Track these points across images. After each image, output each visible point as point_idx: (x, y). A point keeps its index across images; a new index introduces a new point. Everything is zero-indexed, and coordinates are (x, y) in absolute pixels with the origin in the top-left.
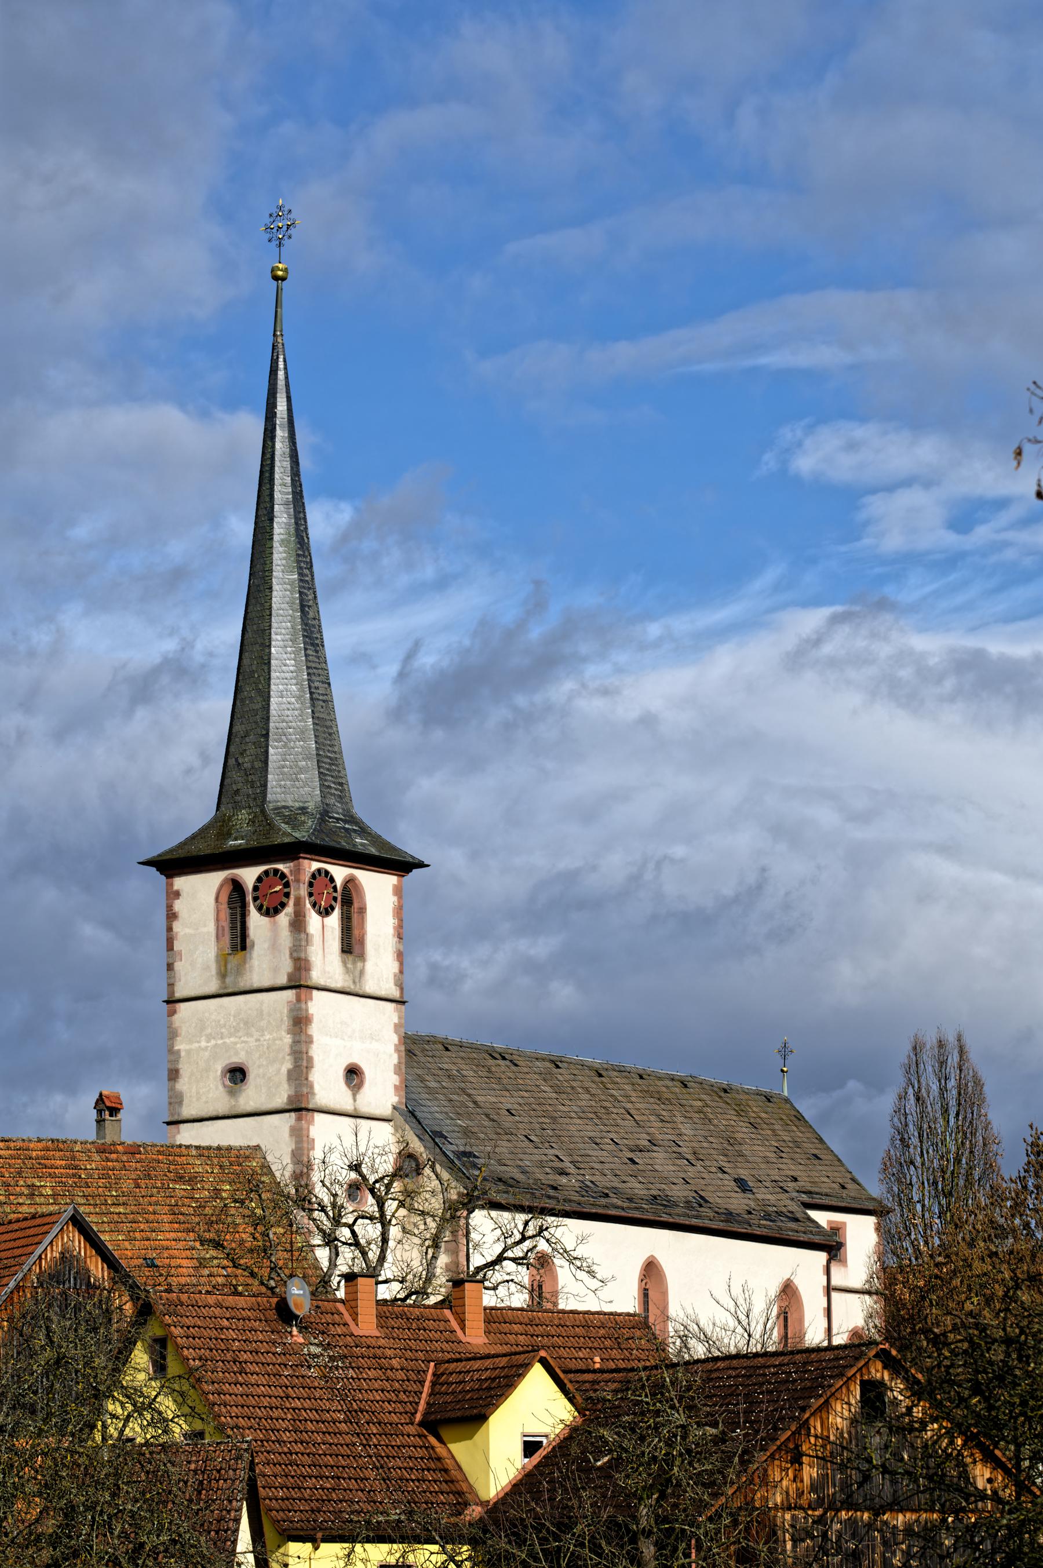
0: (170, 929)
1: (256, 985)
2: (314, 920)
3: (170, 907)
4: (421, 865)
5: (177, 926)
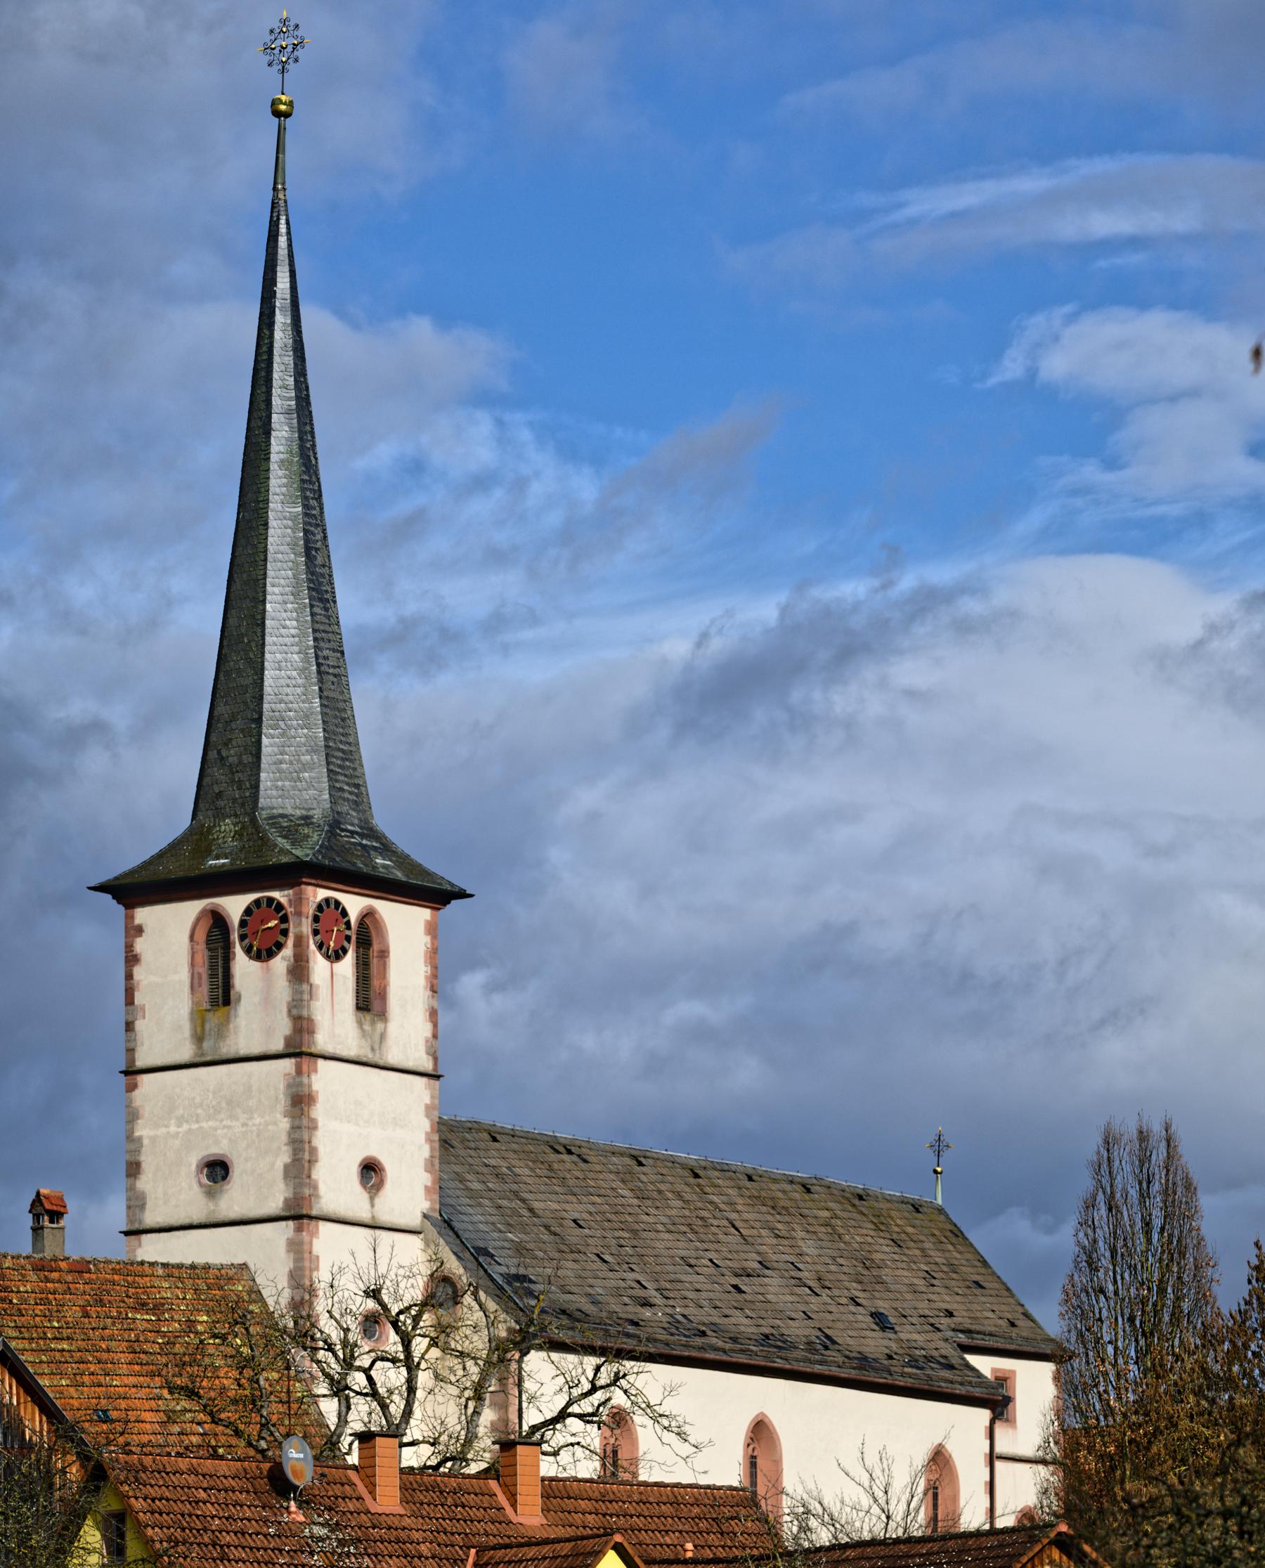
0: (129, 976)
1: (243, 1052)
2: (319, 966)
3: (129, 947)
4: (462, 895)
5: (138, 973)
